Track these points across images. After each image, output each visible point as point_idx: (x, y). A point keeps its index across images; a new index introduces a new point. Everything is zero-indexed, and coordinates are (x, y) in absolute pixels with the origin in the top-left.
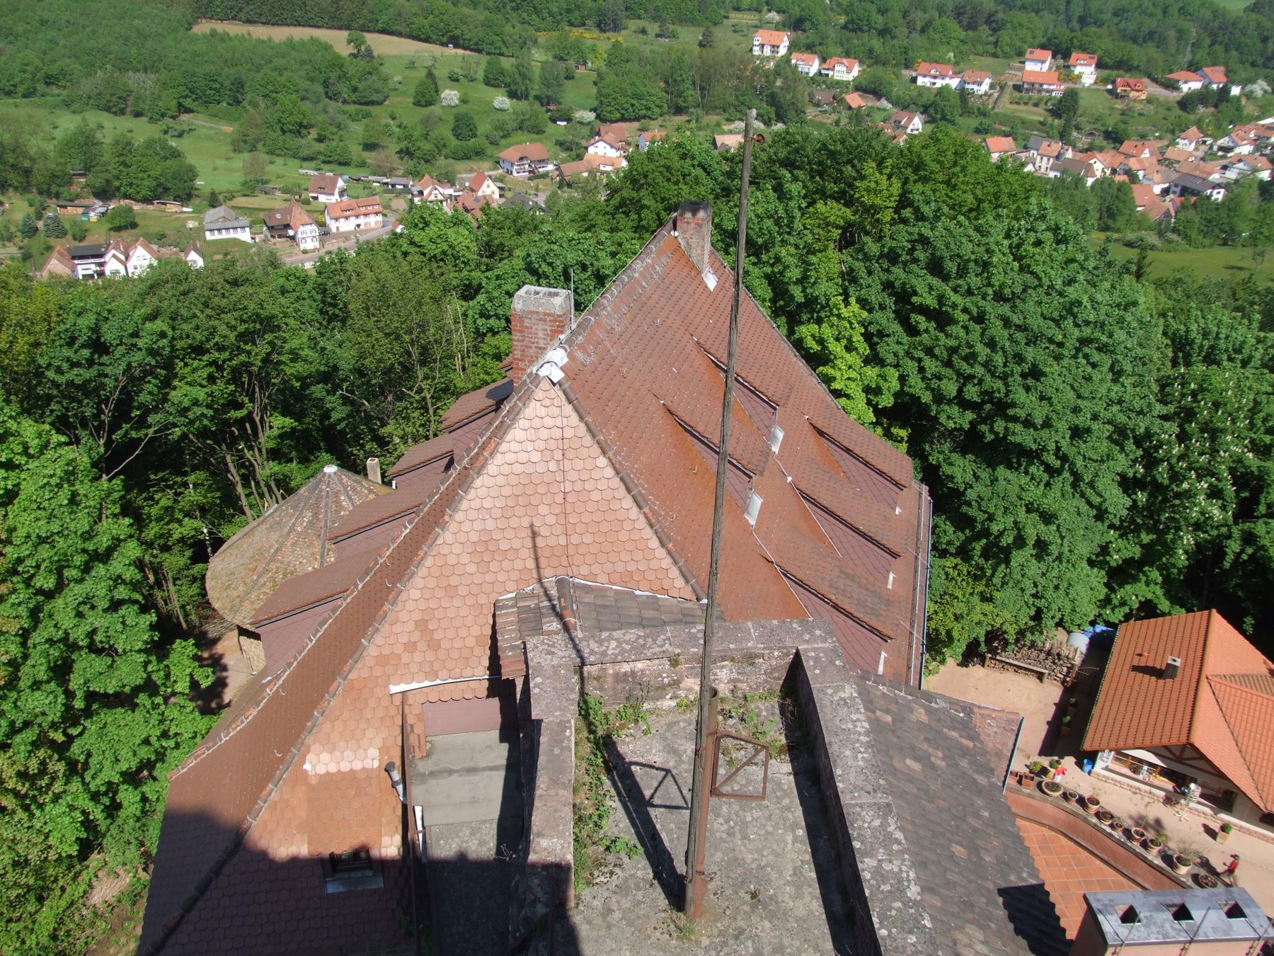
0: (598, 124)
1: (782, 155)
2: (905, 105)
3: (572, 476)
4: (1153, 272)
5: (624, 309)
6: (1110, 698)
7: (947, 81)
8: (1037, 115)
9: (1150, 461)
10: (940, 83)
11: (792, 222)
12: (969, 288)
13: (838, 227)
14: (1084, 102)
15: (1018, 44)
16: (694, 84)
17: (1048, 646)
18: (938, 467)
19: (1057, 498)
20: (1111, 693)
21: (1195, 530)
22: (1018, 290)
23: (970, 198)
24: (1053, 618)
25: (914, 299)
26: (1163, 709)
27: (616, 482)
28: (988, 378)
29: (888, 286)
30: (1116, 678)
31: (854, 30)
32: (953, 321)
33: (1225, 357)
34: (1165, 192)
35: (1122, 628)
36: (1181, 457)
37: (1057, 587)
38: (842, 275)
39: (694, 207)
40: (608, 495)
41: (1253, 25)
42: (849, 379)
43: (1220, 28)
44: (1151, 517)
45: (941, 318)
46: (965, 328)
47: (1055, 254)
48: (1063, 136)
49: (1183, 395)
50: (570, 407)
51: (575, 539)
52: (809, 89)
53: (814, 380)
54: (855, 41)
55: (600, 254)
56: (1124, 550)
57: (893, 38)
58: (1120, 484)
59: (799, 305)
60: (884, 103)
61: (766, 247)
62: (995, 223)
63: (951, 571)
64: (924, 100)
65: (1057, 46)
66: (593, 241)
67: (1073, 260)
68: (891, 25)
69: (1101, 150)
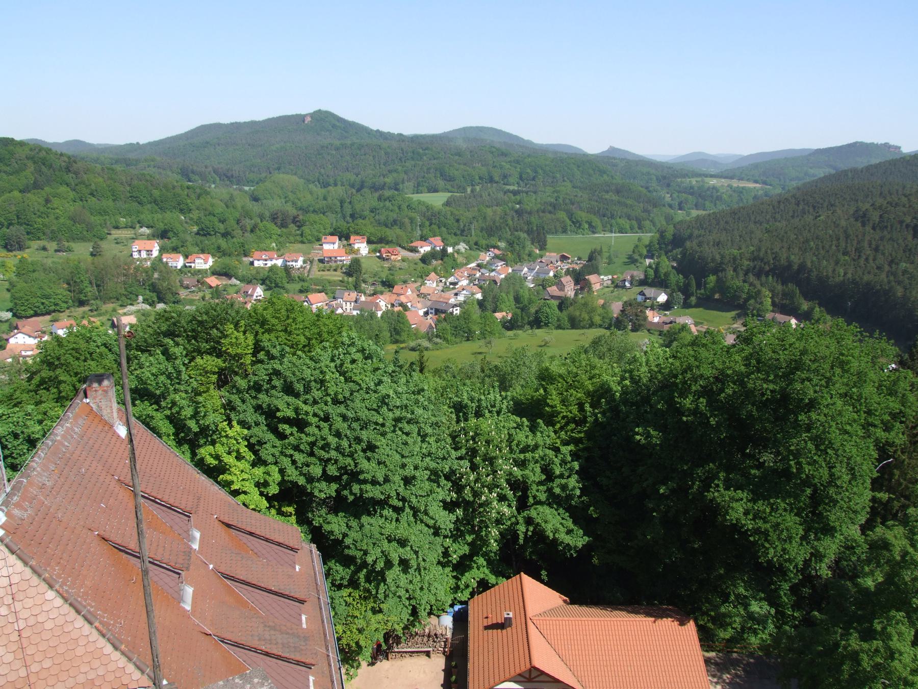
0: (15, 321)
1: (164, 328)
2: (248, 281)
3: (24, 614)
4: (431, 365)
5: (52, 467)
6: (476, 654)
7: (274, 262)
8: (338, 276)
9: (458, 487)
10: (270, 264)
11: (180, 375)
12: (314, 399)
13: (214, 373)
14: (365, 265)
15: (316, 234)
16: (91, 283)
17: (427, 631)
18: (321, 527)
19: (406, 527)
20: (476, 650)
21: (497, 525)
22: (347, 394)
23: (302, 339)
24: (424, 610)
25: (278, 414)
26: (511, 649)
27: (67, 608)
28: (340, 458)
29: (258, 408)
30: (476, 639)
31: (205, 235)
32: (308, 424)
33: (487, 411)
34: (426, 313)
35: (471, 603)
36: (476, 481)
37: (422, 589)
38: (223, 406)
39: (99, 379)
40: (60, 621)
41: (449, 213)
42: (243, 480)
43: (432, 215)
44: (469, 524)
45: (300, 424)
46: (318, 427)
47: (365, 366)
48: (356, 287)
49: (467, 441)
50: (14, 556)
51: (35, 668)
52: (179, 278)
53: (216, 487)
54: (207, 242)
55: (28, 423)
56: (459, 550)
57: (232, 237)
58: (445, 508)
59: (196, 434)
60: (234, 281)
61: (163, 396)
62: (322, 353)
63: (347, 599)
64: (261, 276)
65: (340, 233)
66: (21, 414)
67: (378, 369)
68: (230, 230)
69: (382, 293)
